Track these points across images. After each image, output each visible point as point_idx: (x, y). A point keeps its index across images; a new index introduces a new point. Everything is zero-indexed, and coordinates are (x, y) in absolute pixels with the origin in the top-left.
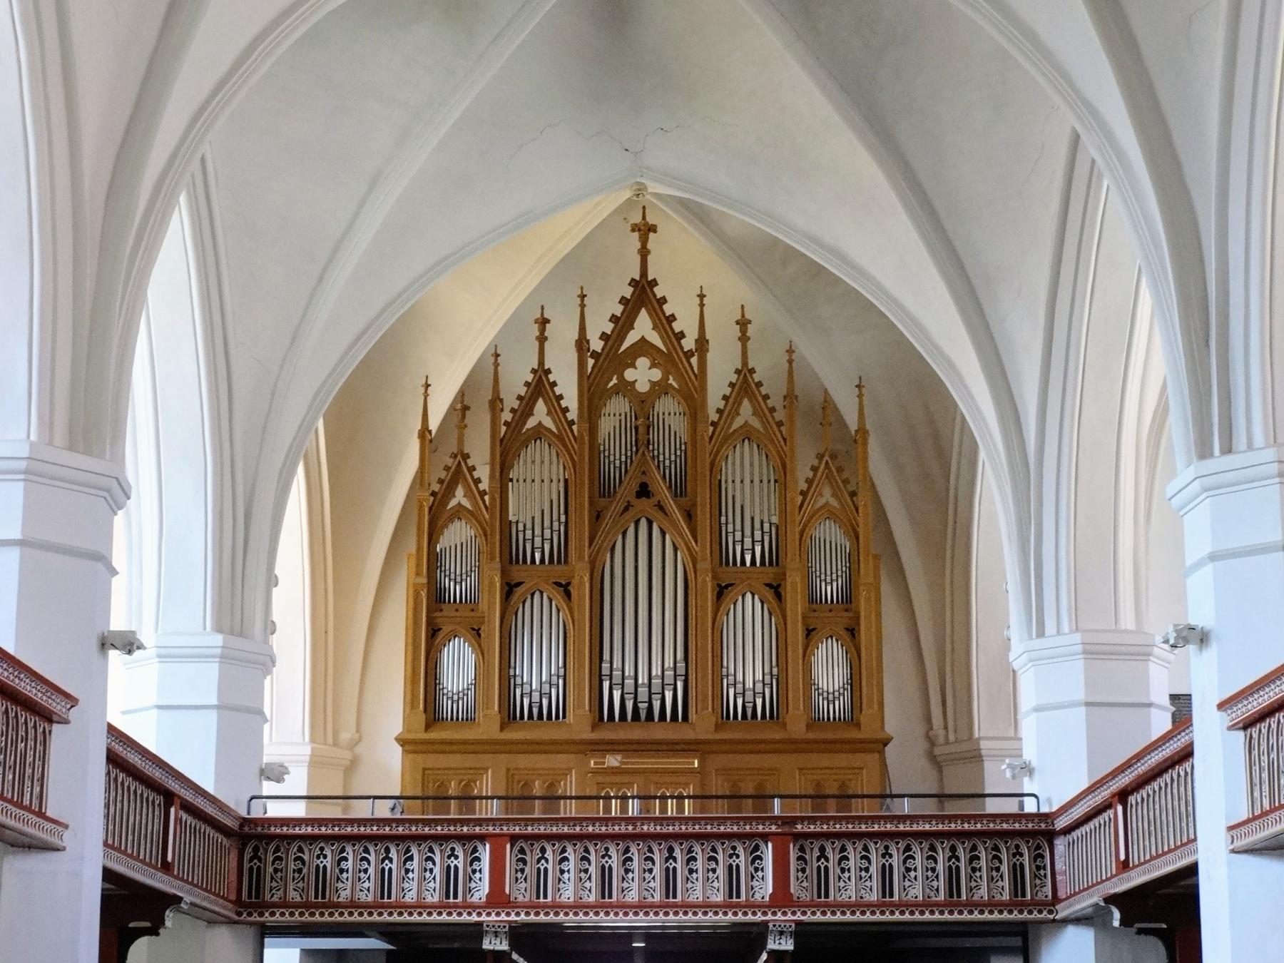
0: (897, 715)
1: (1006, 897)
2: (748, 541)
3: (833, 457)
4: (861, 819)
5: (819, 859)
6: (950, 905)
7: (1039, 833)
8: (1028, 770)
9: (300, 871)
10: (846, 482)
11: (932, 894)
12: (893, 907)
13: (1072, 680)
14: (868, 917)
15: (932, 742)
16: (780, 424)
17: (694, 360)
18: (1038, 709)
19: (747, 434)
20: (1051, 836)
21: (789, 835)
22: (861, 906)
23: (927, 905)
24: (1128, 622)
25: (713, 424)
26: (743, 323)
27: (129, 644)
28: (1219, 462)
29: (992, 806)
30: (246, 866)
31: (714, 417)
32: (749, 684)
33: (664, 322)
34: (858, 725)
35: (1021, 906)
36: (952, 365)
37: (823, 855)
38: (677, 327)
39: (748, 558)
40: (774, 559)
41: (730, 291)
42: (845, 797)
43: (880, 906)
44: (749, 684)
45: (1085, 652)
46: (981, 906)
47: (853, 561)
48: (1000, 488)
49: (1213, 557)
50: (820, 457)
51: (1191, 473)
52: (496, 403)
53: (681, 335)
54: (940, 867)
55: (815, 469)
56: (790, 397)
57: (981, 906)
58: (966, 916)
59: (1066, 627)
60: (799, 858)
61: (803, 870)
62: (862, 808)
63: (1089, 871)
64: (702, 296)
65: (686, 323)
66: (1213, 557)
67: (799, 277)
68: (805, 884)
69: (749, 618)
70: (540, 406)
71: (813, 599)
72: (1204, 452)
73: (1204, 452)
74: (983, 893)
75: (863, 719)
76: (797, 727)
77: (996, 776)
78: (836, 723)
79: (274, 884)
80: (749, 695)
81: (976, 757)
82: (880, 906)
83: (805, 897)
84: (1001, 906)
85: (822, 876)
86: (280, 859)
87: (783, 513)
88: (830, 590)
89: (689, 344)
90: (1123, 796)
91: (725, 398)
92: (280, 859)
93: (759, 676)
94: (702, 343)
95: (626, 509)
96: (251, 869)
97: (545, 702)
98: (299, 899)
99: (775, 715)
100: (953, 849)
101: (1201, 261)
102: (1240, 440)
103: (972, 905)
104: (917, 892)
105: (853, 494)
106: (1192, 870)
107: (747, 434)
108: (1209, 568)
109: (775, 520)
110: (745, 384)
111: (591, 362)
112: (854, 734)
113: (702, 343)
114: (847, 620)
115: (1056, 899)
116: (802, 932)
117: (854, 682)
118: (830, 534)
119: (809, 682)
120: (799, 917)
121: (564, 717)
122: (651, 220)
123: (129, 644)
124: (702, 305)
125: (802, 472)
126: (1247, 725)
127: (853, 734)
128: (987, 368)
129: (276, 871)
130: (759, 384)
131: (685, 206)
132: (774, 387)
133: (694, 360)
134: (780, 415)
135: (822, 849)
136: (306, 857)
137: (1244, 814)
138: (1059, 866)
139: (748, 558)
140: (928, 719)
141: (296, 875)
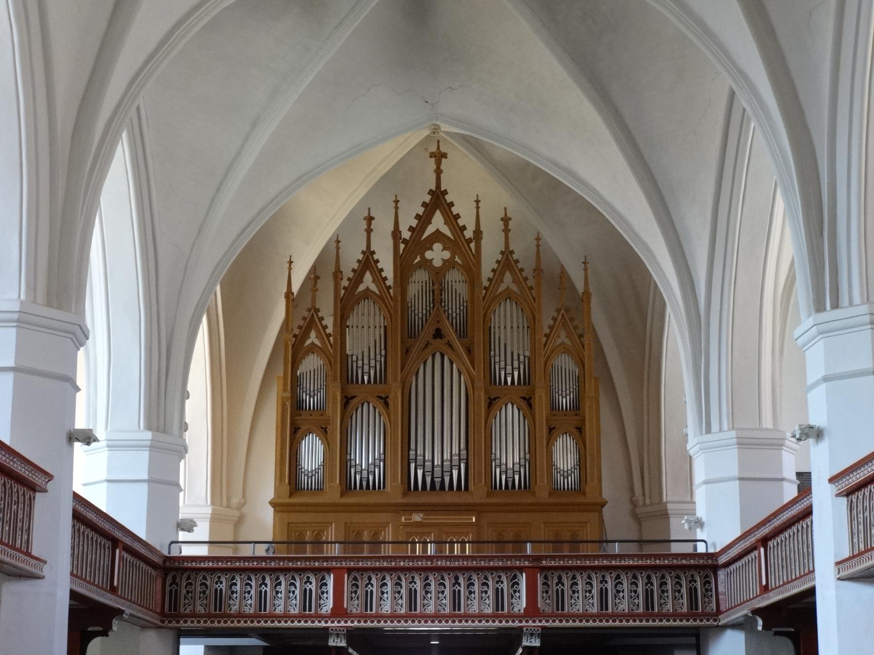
0: (611, 487)
1: (685, 610)
2: (509, 368)
4: (586, 557)
5: (557, 584)
6: (647, 616)
7: (708, 566)
9: (204, 592)
10: (576, 328)
11: (634, 608)
12: (608, 617)
13: (729, 462)
14: (591, 624)
15: (634, 504)
16: (531, 288)
17: (472, 245)
18: (706, 482)
19: (508, 295)
20: (715, 568)
21: (537, 568)
23: (631, 616)
24: (768, 423)
26: (506, 220)
28: (830, 315)
29: (676, 548)
30: (168, 589)
32: (510, 465)
33: (452, 219)
34: (584, 493)
35: (695, 617)
37: (560, 581)
38: (461, 222)
39: (509, 379)
40: (527, 380)
42: (575, 542)
44: (510, 465)
46: (668, 616)
47: (580, 381)
51: (810, 322)
52: (337, 274)
53: (464, 228)
54: (640, 590)
56: (538, 270)
57: (668, 616)
58: (657, 623)
59: (725, 426)
60: (544, 584)
61: (547, 592)
62: (587, 550)
63: (742, 593)
64: (478, 202)
65: (467, 220)
68: (548, 601)
69: (510, 417)
70: (508, 277)
71: (553, 407)
72: (819, 307)
73: (819, 307)
74: (669, 607)
75: (588, 489)
76: (542, 495)
77: (678, 528)
79: (187, 601)
80: (510, 472)
81: (664, 515)
83: (548, 610)
84: (681, 617)
85: (560, 596)
86: (191, 584)
87: (533, 350)
88: (565, 402)
89: (469, 234)
91: (494, 271)
92: (191, 584)
93: (517, 460)
94: (478, 233)
95: (426, 346)
96: (171, 591)
97: (371, 477)
98: (203, 612)
99: (527, 487)
100: (649, 577)
103: (661, 616)
104: (624, 607)
105: (581, 336)
106: (812, 592)
107: (508, 295)
108: (823, 387)
109: (527, 353)
110: (507, 261)
111: (402, 246)
112: (581, 499)
113: (478, 233)
115: (719, 612)
116: (546, 634)
117: (581, 463)
118: (565, 363)
119: (551, 464)
120: (544, 624)
121: (384, 487)
122: (443, 149)
124: (478, 208)
125: (546, 321)
126: (849, 493)
127: (580, 499)
129: (188, 592)
130: (517, 261)
131: (466, 140)
132: (526, 263)
133: (472, 245)
134: (531, 282)
135: (560, 578)
136: (208, 583)
137: (847, 554)
138: (721, 589)
139: (509, 379)
141: (202, 595)
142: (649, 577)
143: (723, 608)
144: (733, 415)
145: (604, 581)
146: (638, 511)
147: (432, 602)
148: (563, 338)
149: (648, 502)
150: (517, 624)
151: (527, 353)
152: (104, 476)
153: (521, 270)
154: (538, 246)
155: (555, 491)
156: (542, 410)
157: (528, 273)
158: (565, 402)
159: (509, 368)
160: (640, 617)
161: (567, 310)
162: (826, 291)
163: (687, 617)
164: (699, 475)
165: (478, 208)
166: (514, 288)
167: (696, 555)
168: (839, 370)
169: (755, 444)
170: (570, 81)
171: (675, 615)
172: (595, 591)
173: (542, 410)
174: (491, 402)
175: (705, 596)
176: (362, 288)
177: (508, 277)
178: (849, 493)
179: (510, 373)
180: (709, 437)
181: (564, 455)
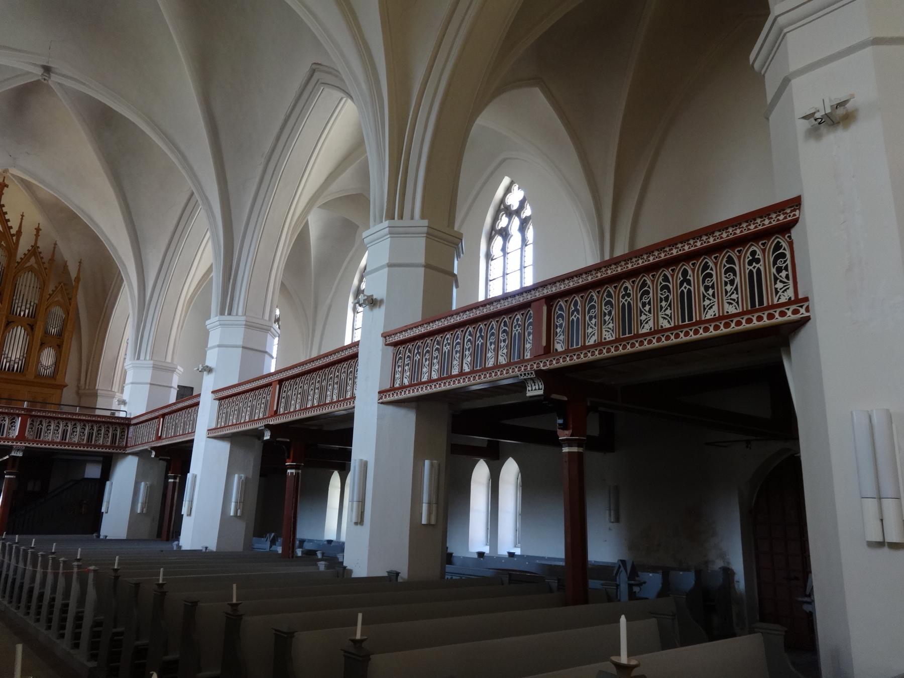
0: (70, 378)
1: (109, 444)
2: (23, 308)
3: (65, 284)
4: (49, 412)
6: (87, 445)
7: (126, 424)
8: (124, 403)
10: (68, 294)
12: (65, 444)
13: (147, 375)
14: (55, 447)
15: (78, 387)
16: (46, 269)
17: (14, 238)
18: (132, 383)
19: (31, 269)
20: (129, 425)
21: (27, 415)
22: (53, 443)
23: (79, 444)
24: (169, 359)
25: (18, 263)
26: (38, 230)
27: (210, 370)
28: (226, 317)
29: (98, 412)
31: (18, 260)
32: (13, 358)
34: (55, 379)
35: (114, 448)
36: (124, 265)
37: (41, 423)
38: (9, 224)
39: (22, 314)
40: (34, 316)
41: (34, 217)
42: (45, 403)
43: (60, 443)
44: (13, 358)
45: (427, 233)
46: (99, 446)
47: (65, 323)
48: (133, 309)
49: (219, 346)
50: (60, 283)
51: (217, 318)
53: (11, 227)
54: (86, 432)
55: (56, 288)
56: (52, 260)
57: (99, 446)
58: (93, 449)
59: (148, 358)
62: (53, 408)
63: (145, 438)
64: (23, 216)
66: (219, 346)
67: (66, 218)
69: (19, 335)
70: (33, 260)
71: (46, 332)
72: (222, 313)
73: (222, 313)
74: (101, 442)
75: (58, 377)
76: (30, 377)
77: (101, 403)
78: (47, 377)
80: (12, 363)
81: (95, 395)
82: (60, 443)
83: (30, 438)
84: (106, 447)
85: (39, 432)
87: (40, 300)
88: (53, 331)
89: (13, 231)
90: (163, 416)
91: (25, 254)
93: (18, 356)
94: (19, 232)
99: (22, 371)
100: (92, 426)
101: (232, 254)
102: (234, 312)
103: (95, 446)
104: (76, 440)
105: (70, 299)
106: (192, 441)
107: (31, 269)
108: (217, 349)
109: (36, 302)
110: (34, 251)
112: (54, 382)
113: (19, 232)
114: (59, 344)
115: (126, 446)
116: (27, 450)
117: (57, 363)
118: (58, 311)
119: (38, 361)
120: (27, 444)
122: (6, 182)
123: (210, 370)
124: (22, 219)
125: (51, 287)
126: (220, 399)
127: (53, 382)
128: (137, 267)
130: (40, 253)
131: (27, 185)
132: (46, 256)
133: (14, 238)
134: (46, 265)
135: (41, 422)
137: (214, 426)
138: (130, 435)
139: (22, 314)
140: (79, 380)
142: (92, 426)
143: (129, 445)
144: (153, 353)
145: (66, 425)
146: (81, 392)
147: (51, 435)
148: (59, 298)
149: (282, 411)
150: (10, 443)
151: (36, 302)
152: (149, 381)
153: (42, 258)
154: (54, 248)
155: (38, 375)
156: (39, 333)
157: (46, 260)
158: (53, 331)
159: (23, 308)
160: (84, 445)
161: (65, 284)
162: (227, 307)
163: (109, 447)
164: (129, 379)
165: (22, 219)
166: (35, 266)
167: (113, 417)
168: (226, 343)
169: (162, 369)
170: (104, 174)
171: (103, 446)
172: (60, 431)
173: (39, 333)
174: (8, 324)
175: (120, 438)
176: (28, 264)
177: (33, 260)
178: (220, 399)
179: (24, 311)
180: (138, 362)
181: (47, 358)
